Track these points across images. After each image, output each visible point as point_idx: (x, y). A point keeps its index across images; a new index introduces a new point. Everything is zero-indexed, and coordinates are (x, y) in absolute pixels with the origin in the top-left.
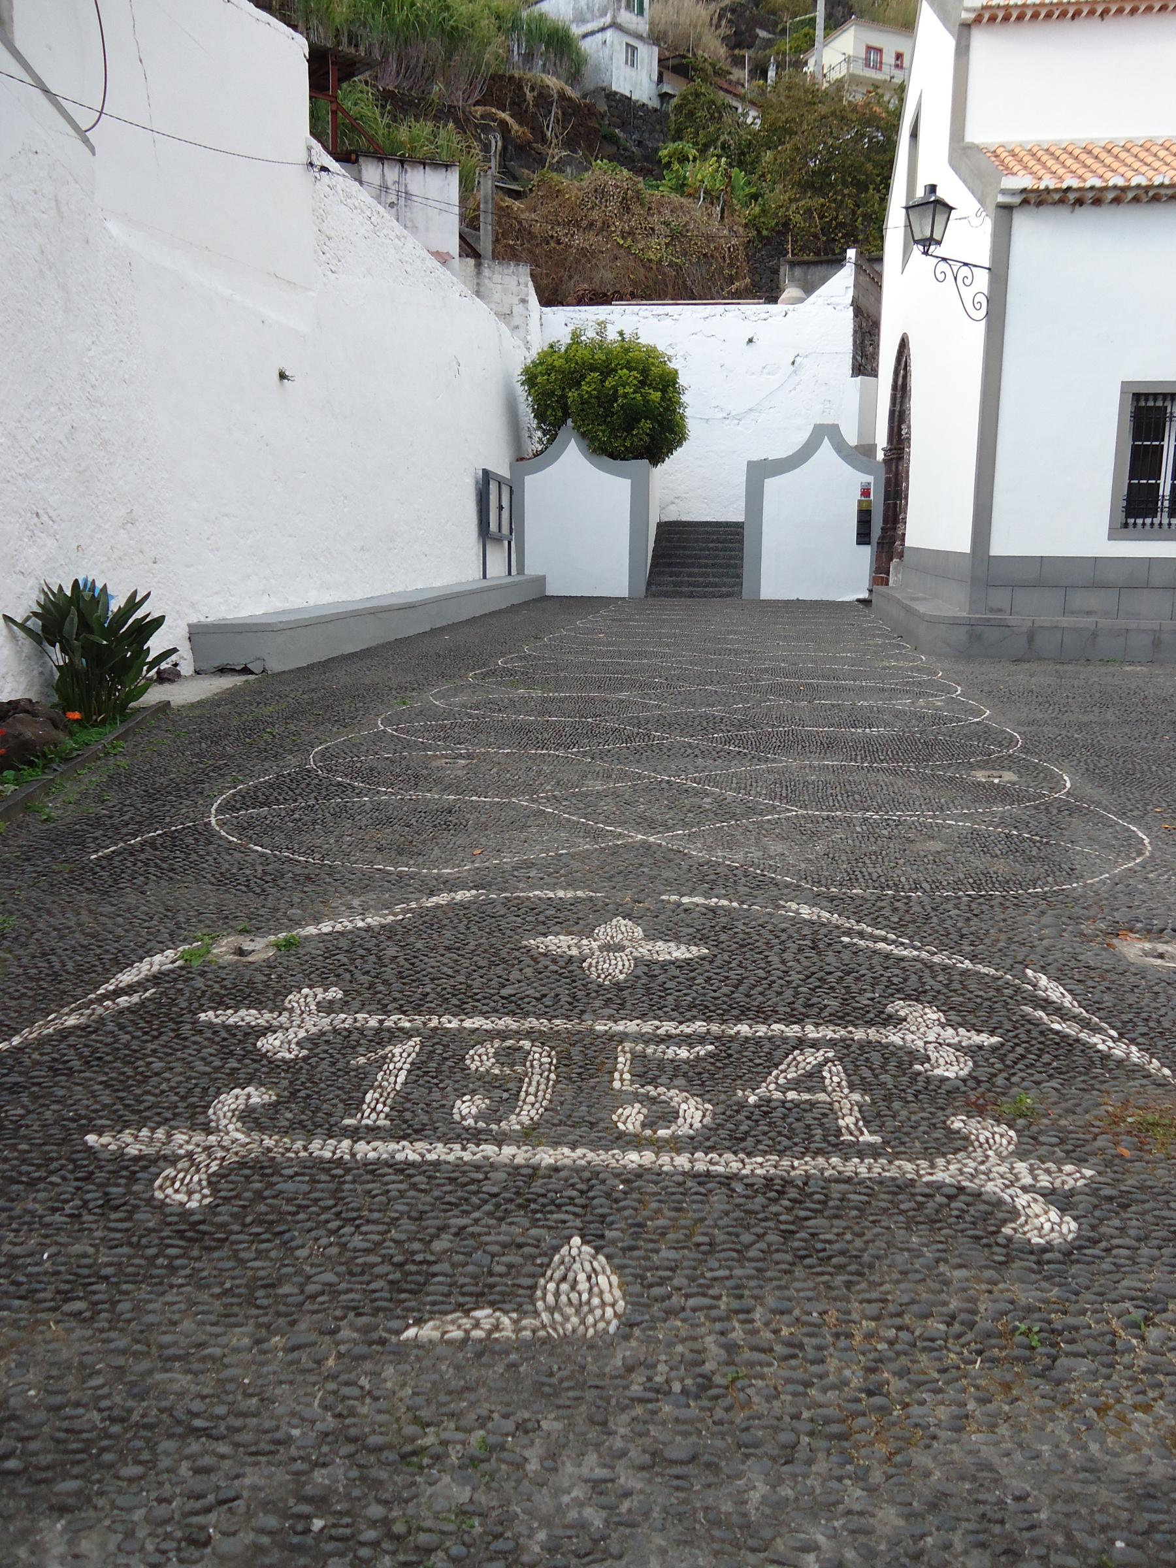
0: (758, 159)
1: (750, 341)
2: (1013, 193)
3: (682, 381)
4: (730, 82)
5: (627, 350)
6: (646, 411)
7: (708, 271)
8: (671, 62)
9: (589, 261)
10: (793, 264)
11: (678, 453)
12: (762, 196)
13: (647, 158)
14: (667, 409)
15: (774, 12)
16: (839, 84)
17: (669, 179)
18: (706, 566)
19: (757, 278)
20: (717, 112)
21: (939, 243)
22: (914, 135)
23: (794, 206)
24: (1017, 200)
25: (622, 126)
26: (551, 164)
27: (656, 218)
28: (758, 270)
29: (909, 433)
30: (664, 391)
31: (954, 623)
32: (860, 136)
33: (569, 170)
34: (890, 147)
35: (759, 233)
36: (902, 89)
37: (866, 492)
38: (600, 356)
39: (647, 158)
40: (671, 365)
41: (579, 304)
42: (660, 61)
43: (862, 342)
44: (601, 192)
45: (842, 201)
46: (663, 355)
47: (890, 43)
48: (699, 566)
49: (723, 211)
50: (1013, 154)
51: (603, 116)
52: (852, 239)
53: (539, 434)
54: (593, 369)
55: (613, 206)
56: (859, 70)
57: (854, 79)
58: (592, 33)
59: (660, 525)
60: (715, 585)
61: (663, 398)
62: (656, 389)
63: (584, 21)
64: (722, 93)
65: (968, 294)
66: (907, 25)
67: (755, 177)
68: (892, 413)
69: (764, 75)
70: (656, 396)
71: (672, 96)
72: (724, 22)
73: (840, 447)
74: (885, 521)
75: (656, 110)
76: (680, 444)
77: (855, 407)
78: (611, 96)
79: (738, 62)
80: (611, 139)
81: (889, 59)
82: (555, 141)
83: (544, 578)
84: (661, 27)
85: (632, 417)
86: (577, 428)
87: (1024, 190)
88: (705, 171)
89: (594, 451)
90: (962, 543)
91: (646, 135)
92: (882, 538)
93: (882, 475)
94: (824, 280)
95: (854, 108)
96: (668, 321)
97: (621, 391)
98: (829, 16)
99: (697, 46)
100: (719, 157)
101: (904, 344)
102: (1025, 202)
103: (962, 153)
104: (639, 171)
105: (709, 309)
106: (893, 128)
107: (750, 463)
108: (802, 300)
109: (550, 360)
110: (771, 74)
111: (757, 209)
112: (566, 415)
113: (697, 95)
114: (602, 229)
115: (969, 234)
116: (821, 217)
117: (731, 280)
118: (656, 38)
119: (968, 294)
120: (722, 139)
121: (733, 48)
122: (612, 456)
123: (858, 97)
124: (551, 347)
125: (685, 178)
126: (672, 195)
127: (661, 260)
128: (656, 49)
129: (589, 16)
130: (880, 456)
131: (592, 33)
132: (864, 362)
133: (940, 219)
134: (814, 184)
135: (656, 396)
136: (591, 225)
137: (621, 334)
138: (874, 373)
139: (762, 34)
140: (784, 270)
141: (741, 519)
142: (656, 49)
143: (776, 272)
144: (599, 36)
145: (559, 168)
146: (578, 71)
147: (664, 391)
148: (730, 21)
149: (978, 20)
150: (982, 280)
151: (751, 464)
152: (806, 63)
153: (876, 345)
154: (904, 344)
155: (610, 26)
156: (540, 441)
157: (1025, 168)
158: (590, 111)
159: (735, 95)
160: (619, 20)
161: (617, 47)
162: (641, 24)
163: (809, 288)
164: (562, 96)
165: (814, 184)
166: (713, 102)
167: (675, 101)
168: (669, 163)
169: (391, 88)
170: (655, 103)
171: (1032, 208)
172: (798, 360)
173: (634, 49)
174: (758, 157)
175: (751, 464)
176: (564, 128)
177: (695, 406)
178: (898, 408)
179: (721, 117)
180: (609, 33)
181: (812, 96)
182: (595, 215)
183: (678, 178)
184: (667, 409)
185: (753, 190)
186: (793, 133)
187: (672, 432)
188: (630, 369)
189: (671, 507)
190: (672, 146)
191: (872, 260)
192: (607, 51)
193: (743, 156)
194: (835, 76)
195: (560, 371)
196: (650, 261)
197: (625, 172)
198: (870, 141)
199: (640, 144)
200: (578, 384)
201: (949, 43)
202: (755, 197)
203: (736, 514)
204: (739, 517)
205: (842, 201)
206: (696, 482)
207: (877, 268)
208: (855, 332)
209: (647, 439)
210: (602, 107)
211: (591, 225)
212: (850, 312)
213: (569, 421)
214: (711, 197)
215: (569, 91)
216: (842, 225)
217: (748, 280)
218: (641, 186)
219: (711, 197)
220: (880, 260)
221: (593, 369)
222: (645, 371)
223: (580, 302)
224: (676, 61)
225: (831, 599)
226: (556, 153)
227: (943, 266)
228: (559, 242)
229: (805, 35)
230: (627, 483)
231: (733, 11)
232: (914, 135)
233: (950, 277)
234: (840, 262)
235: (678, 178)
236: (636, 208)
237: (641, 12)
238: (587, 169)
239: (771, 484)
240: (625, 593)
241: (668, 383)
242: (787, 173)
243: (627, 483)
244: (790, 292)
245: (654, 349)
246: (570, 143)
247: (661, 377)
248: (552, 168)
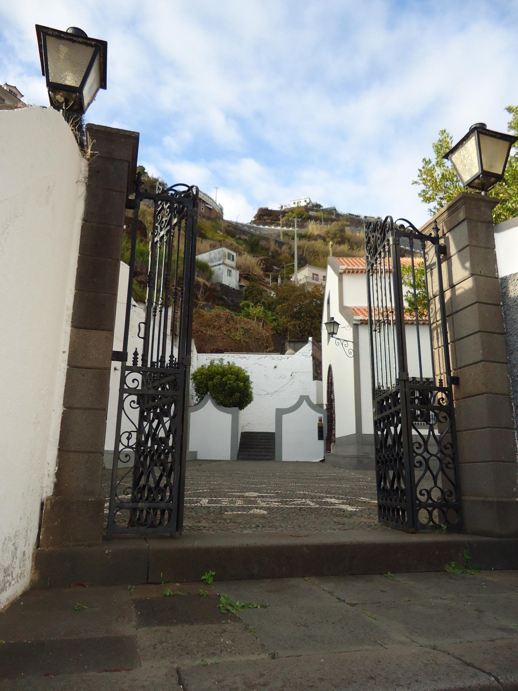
0: (275, 307)
1: (275, 367)
2: (358, 321)
3: (251, 379)
5: (231, 368)
6: (238, 389)
8: (243, 276)
9: (213, 339)
10: (290, 342)
11: (249, 406)
14: (245, 389)
16: (304, 285)
19: (276, 347)
20: (261, 293)
21: (336, 334)
22: (328, 303)
23: (289, 323)
24: (359, 323)
25: (226, 295)
28: (279, 342)
29: (334, 397)
30: (244, 383)
31: (352, 457)
32: (312, 302)
33: (206, 308)
35: (277, 331)
36: (324, 288)
37: (320, 420)
38: (220, 369)
40: (247, 374)
41: (211, 353)
42: (240, 275)
43: (316, 369)
44: (218, 316)
45: (306, 322)
47: (320, 273)
49: (263, 324)
50: (359, 310)
51: (219, 291)
53: (197, 397)
54: (218, 374)
55: (223, 321)
56: (310, 280)
57: (309, 283)
58: (215, 266)
59: (242, 433)
60: (264, 456)
61: (244, 385)
62: (241, 382)
64: (262, 286)
66: (325, 268)
67: (274, 313)
68: (328, 392)
69: (277, 281)
70: (241, 384)
72: (262, 264)
73: (310, 404)
75: (238, 290)
76: (250, 402)
78: (222, 285)
79: (268, 276)
82: (201, 299)
84: (240, 264)
85: (232, 392)
86: (211, 395)
87: (361, 320)
88: (258, 310)
95: (309, 293)
96: (245, 360)
97: (228, 382)
98: (299, 264)
99: (252, 270)
100: (261, 306)
101: (330, 368)
102: (362, 323)
103: (343, 309)
104: (232, 310)
105: (260, 356)
106: (322, 300)
107: (277, 409)
108: (293, 354)
109: (202, 371)
110: (279, 280)
111: (276, 324)
113: (253, 287)
114: (218, 329)
115: (345, 331)
116: (299, 327)
117: (267, 348)
118: (238, 267)
119: (347, 349)
120: (262, 301)
123: (310, 289)
125: (249, 313)
126: (245, 318)
127: (240, 340)
128: (238, 272)
129: (214, 260)
130: (325, 407)
131: (215, 266)
132: (317, 375)
133: (336, 327)
134: (296, 316)
135: (241, 384)
136: (214, 327)
137: (229, 362)
139: (275, 268)
140: (287, 344)
142: (238, 272)
143: (284, 345)
144: (218, 267)
145: (203, 307)
146: (210, 277)
147: (244, 383)
148: (263, 264)
149: (345, 272)
150: (351, 346)
151: (277, 410)
152: (292, 277)
153: (321, 369)
154: (330, 368)
155: (222, 264)
157: (363, 314)
158: (214, 290)
159: (267, 287)
160: (225, 262)
161: (224, 270)
162: (233, 264)
163: (296, 350)
164: (205, 285)
165: (296, 316)
167: (245, 288)
168: (243, 307)
169: (143, 280)
171: (364, 326)
172: (293, 374)
173: (230, 271)
175: (277, 410)
177: (249, 408)
178: (330, 390)
179: (262, 293)
180: (221, 266)
181: (294, 288)
182: (216, 324)
184: (245, 389)
185: (274, 318)
186: (287, 300)
187: (247, 398)
189: (246, 427)
191: (317, 342)
192: (221, 271)
193: (269, 306)
194: (302, 282)
195: (206, 374)
196: (236, 340)
197: (227, 310)
198: (315, 303)
199: (232, 301)
201: (336, 278)
203: (271, 428)
204: (273, 431)
205: (306, 322)
206: (256, 418)
208: (313, 365)
210: (219, 288)
212: (311, 358)
213: (208, 393)
214: (259, 319)
215: (207, 283)
216: (306, 330)
217: (273, 348)
218: (233, 315)
219: (259, 319)
220: (320, 341)
221: (218, 374)
222: (237, 376)
223: (212, 352)
224: (246, 275)
225: (310, 461)
226: (202, 303)
228: (202, 332)
229: (291, 269)
231: (265, 260)
232: (328, 303)
234: (306, 342)
236: (231, 322)
237: (233, 260)
238: (213, 309)
239: (285, 417)
240: (228, 458)
244: (289, 351)
245: (241, 368)
246: (207, 300)
248: (200, 308)
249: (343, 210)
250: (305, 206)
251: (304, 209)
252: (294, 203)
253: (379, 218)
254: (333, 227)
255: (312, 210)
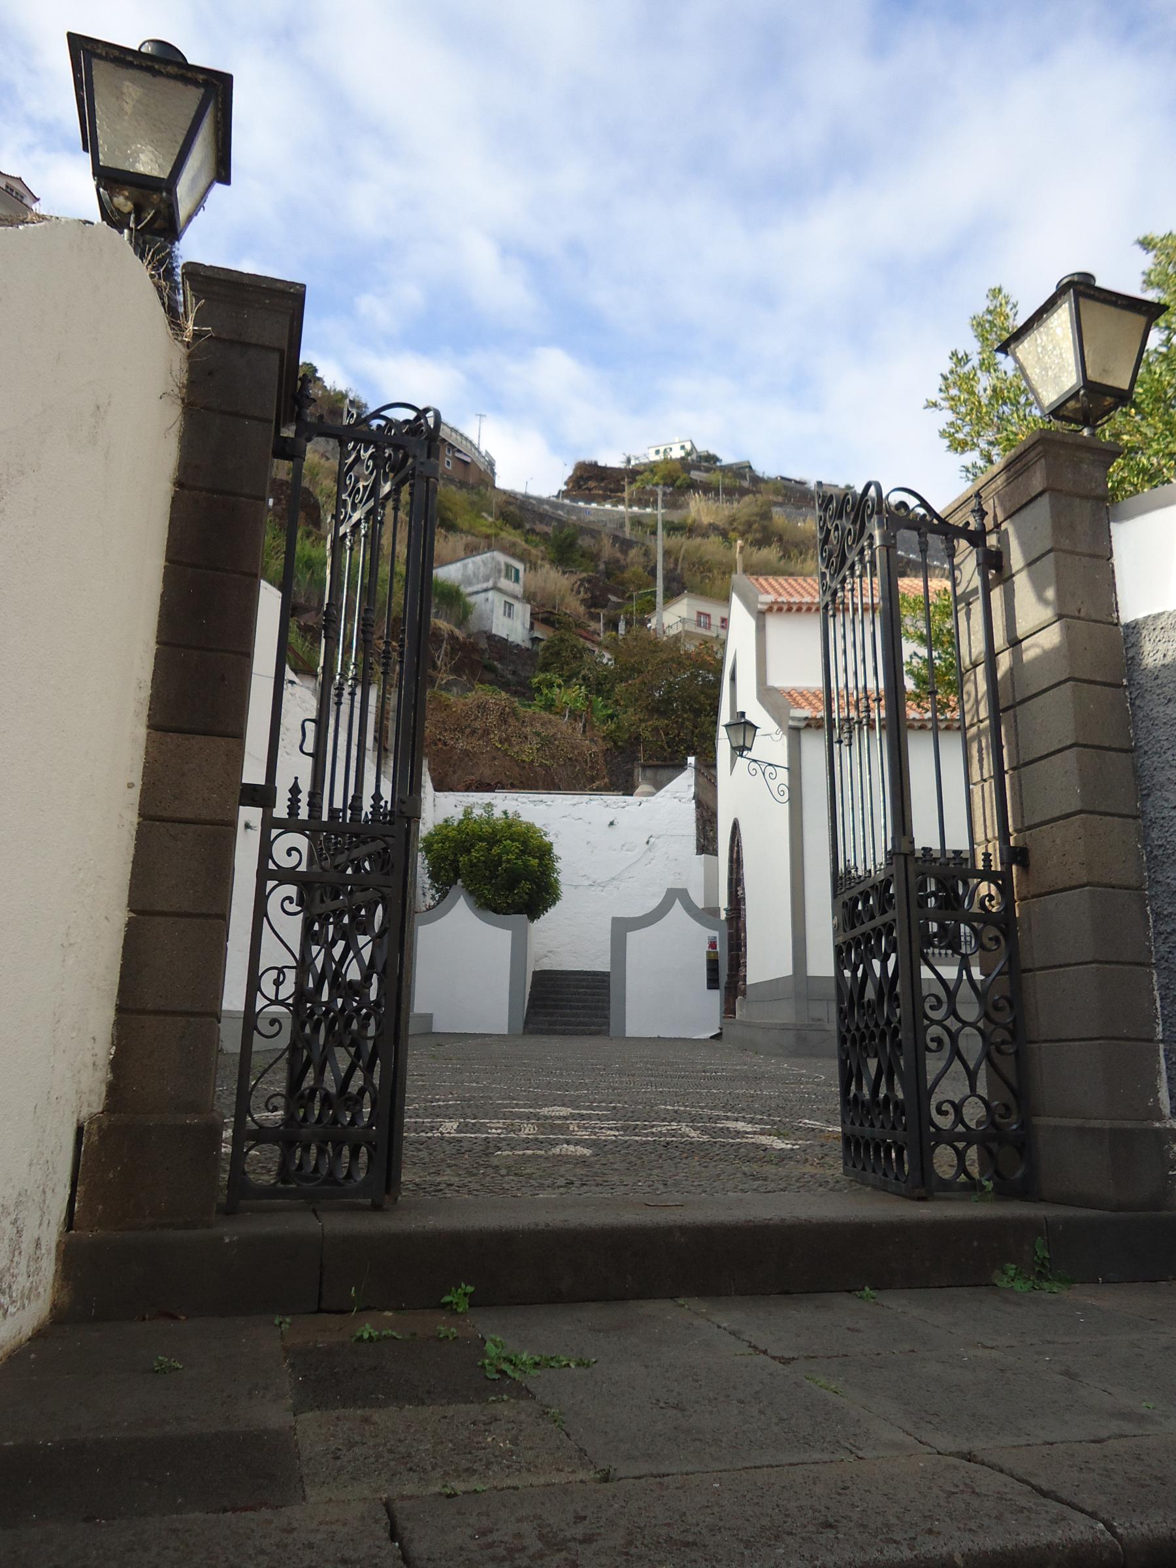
1: (612, 824)
2: (799, 719)
3: (556, 851)
4: (588, 632)
5: (510, 826)
7: (573, 772)
10: (644, 767)
11: (552, 911)
12: (617, 716)
13: (520, 684)
14: (543, 873)
15: (622, 583)
16: (677, 638)
17: (539, 700)
18: (577, 1008)
20: (579, 654)
22: (733, 678)
24: (802, 724)
26: (440, 685)
27: (528, 729)
29: (744, 893)
30: (541, 858)
31: (784, 1028)
32: (694, 676)
33: (455, 689)
34: (718, 684)
35: (615, 743)
36: (723, 644)
37: (713, 945)
38: (487, 829)
39: (520, 684)
40: (546, 839)
43: (704, 828)
44: (483, 708)
46: (540, 830)
47: (716, 612)
48: (572, 1008)
49: (584, 726)
50: (802, 695)
51: (484, 651)
52: (691, 751)
54: (481, 839)
55: (492, 719)
56: (692, 628)
57: (688, 634)
58: (477, 593)
59: (535, 973)
60: (586, 1024)
61: (540, 865)
62: (534, 857)
63: (470, 584)
64: (582, 640)
65: (774, 785)
66: (727, 600)
69: (616, 627)
71: (542, 640)
73: (690, 907)
74: (730, 969)
75: (528, 649)
77: (700, 878)
78: (491, 637)
79: (595, 617)
80: (490, 669)
81: (715, 621)
83: (431, 1016)
84: (532, 589)
85: (513, 879)
86: (466, 886)
87: (806, 718)
88: (572, 695)
89: (480, 906)
90: (787, 970)
91: (520, 667)
92: (728, 983)
93: (726, 931)
94: (670, 780)
95: (688, 656)
96: (542, 807)
98: (667, 589)
100: (581, 686)
101: (735, 827)
102: (808, 726)
103: (766, 694)
104: (515, 693)
106: (719, 672)
107: (614, 919)
108: (653, 794)
110: (622, 626)
112: (458, 875)
113: (562, 640)
115: (771, 743)
116: (667, 734)
118: (528, 597)
119: (774, 785)
120: (583, 673)
121: (591, 607)
122: (496, 911)
123: (691, 647)
124: (446, 821)
127: (532, 761)
128: (528, 607)
130: (723, 915)
131: (477, 593)
132: (706, 844)
133: (749, 734)
134: (660, 709)
137: (505, 813)
138: (715, 853)
139: (613, 598)
140: (638, 771)
141: (609, 970)
142: (528, 607)
144: (483, 595)
145: (447, 687)
147: (541, 858)
149: (770, 609)
150: (783, 776)
151: (615, 921)
153: (715, 830)
154: (735, 827)
156: (433, 898)
161: (497, 603)
162: (518, 589)
163: (659, 786)
164: (452, 636)
165: (660, 709)
166: (575, 646)
167: (542, 644)
170: (528, 645)
171: (813, 731)
172: (652, 840)
173: (511, 605)
174: (613, 687)
175: (615, 921)
176: (452, 659)
177: (552, 915)
179: (582, 657)
180: (490, 594)
181: (654, 645)
182: (477, 725)
183: (547, 699)
184: (543, 873)
185: (610, 711)
188: (513, 840)
190: (542, 676)
191: (707, 767)
192: (489, 606)
193: (599, 686)
194: (673, 632)
195: (453, 840)
196: (523, 761)
197: (503, 694)
198: (703, 680)
199: (514, 673)
200: (469, 852)
201: (751, 623)
202: (611, 717)
203: (602, 964)
205: (683, 723)
206: (567, 937)
207: (712, 772)
208: (698, 820)
209: (526, 897)
210: (483, 645)
211: (473, 732)
212: (693, 804)
213: (459, 882)
215: (457, 632)
216: (682, 741)
217: (606, 780)
218: (516, 704)
219: (575, 715)
220: (715, 766)
221: (481, 839)
222: (524, 843)
223: (468, 789)
224: (545, 615)
226: (444, 677)
227: (753, 765)
228: (445, 744)
230: (507, 935)
231: (589, 581)
232: (733, 678)
233: (760, 773)
234: (682, 767)
235: (547, 699)
236: (511, 720)
237: (517, 580)
239: (633, 937)
241: (544, 853)
242: (637, 700)
243: (507, 935)
244: (643, 788)
246: (457, 670)
247: (539, 848)
248: (441, 688)
249: (766, 467)
250: (682, 459)
251: (678, 466)
252: (657, 452)
253: (848, 487)
254: (744, 507)
255: (698, 468)
